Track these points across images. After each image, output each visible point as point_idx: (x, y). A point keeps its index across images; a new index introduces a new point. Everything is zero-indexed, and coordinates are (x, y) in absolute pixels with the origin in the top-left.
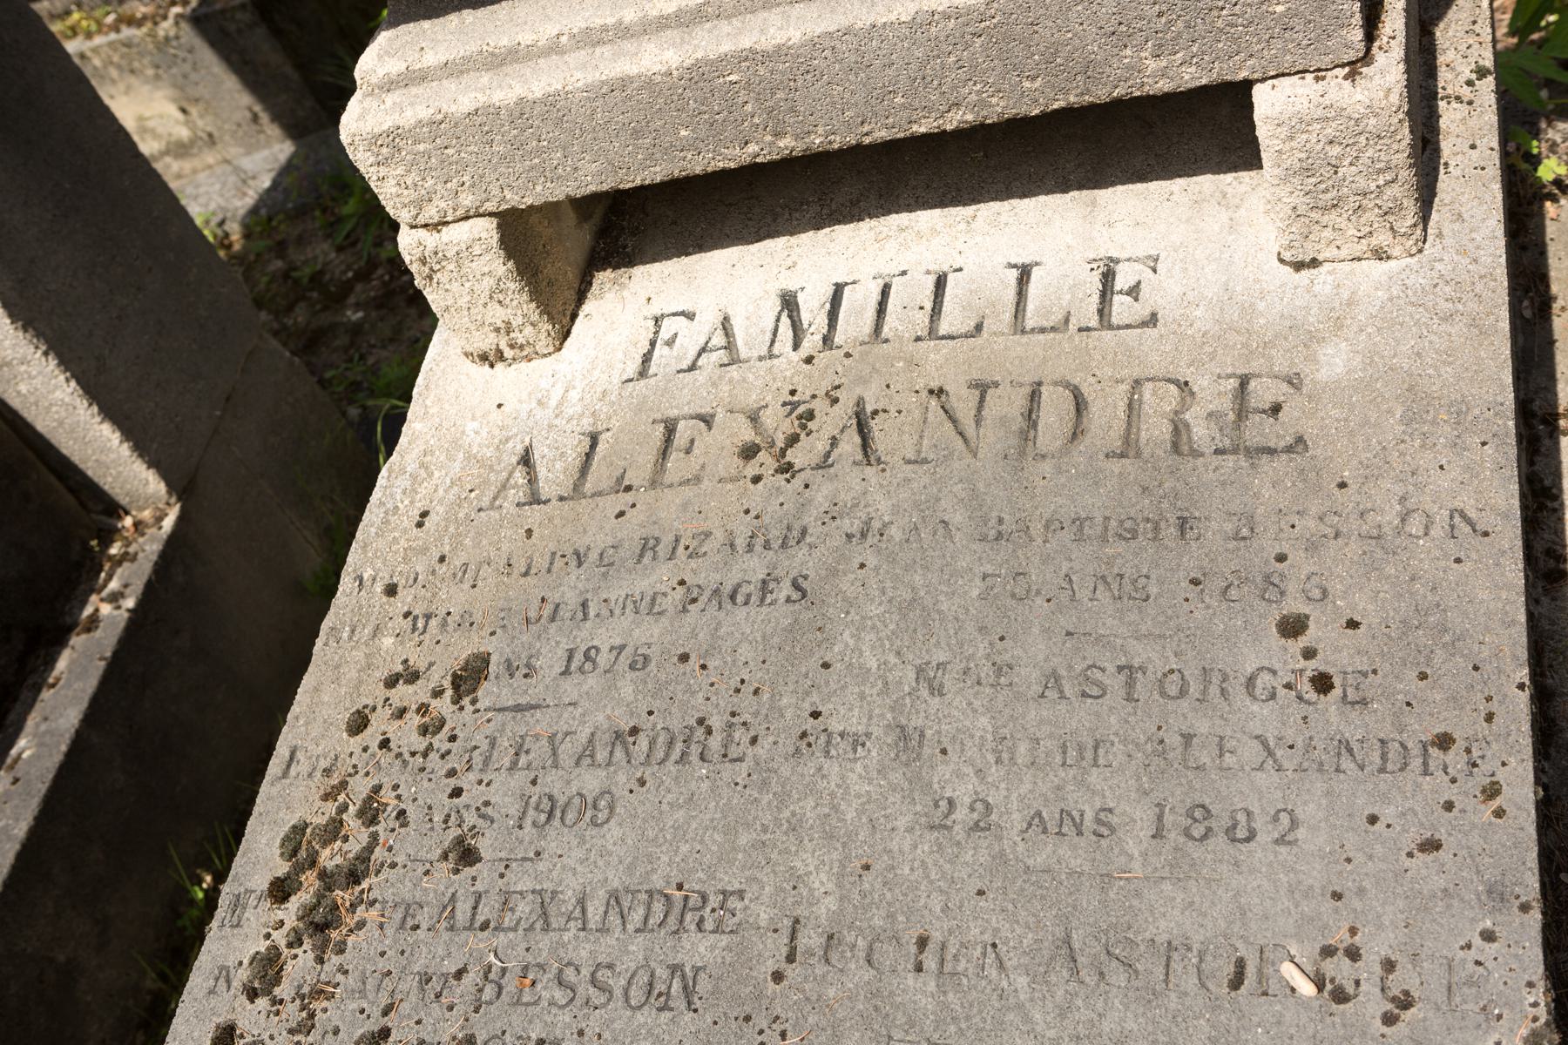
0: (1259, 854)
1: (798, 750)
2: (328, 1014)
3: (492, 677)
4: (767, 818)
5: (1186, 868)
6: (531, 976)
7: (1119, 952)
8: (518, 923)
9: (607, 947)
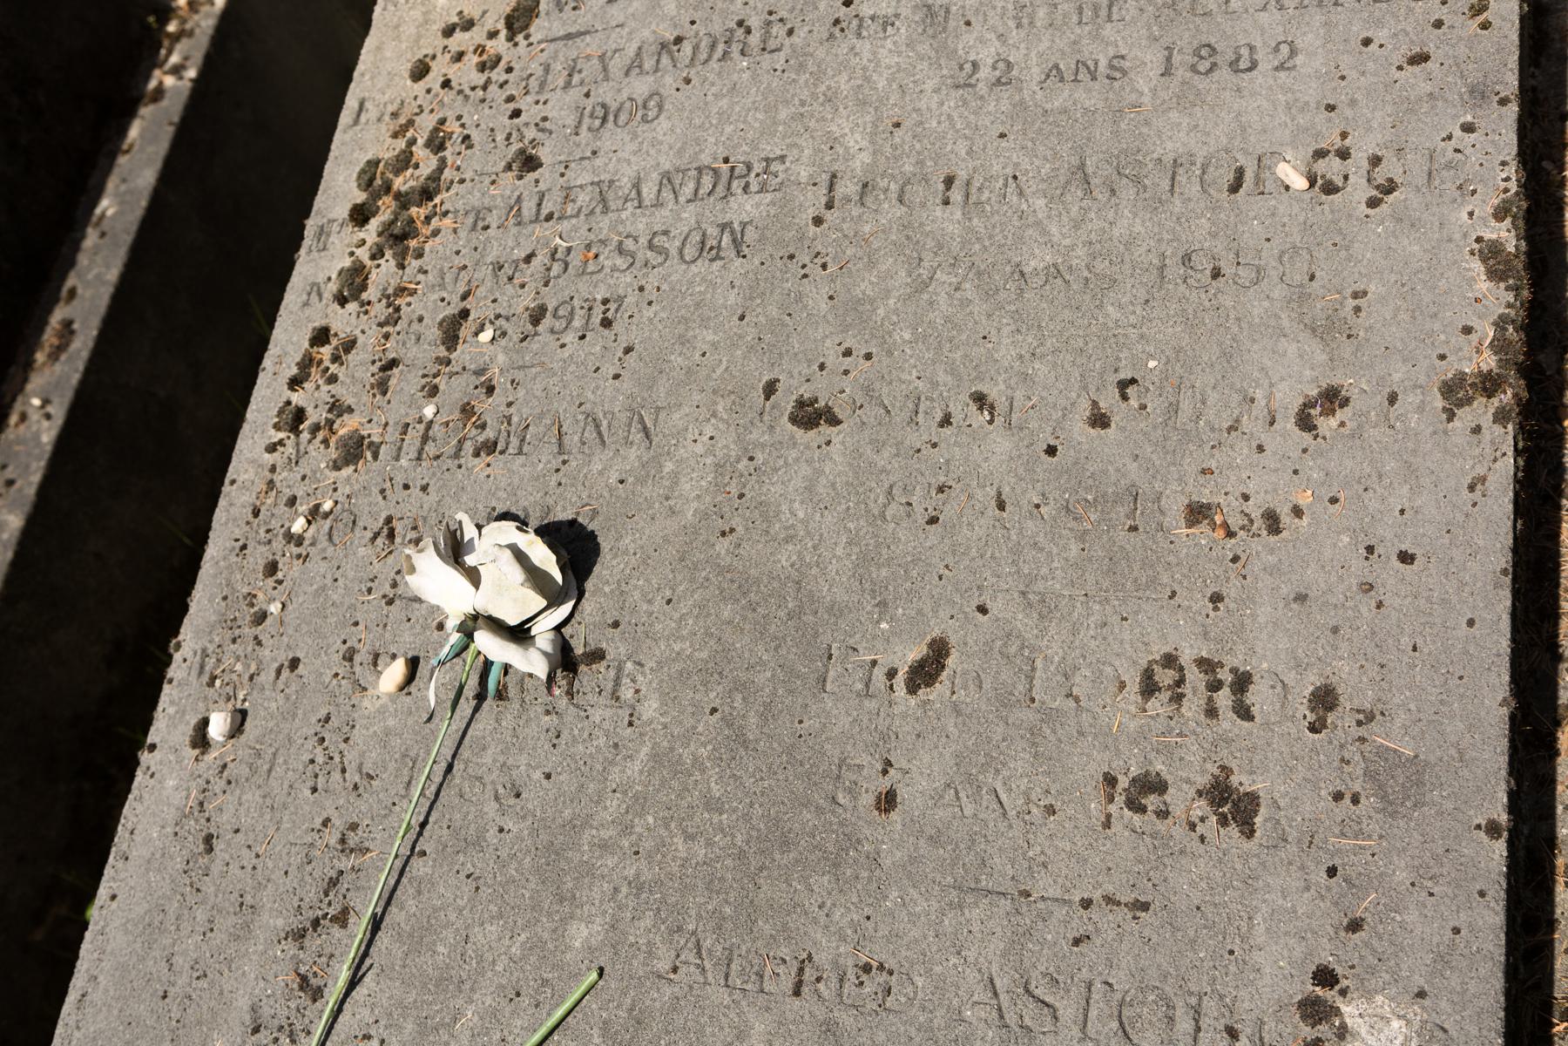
0: (1260, 80)
1: (832, 36)
2: (411, 307)
3: (542, 14)
4: (805, 95)
5: (1191, 98)
6: (594, 251)
7: (1128, 169)
8: (580, 210)
9: (661, 218)
